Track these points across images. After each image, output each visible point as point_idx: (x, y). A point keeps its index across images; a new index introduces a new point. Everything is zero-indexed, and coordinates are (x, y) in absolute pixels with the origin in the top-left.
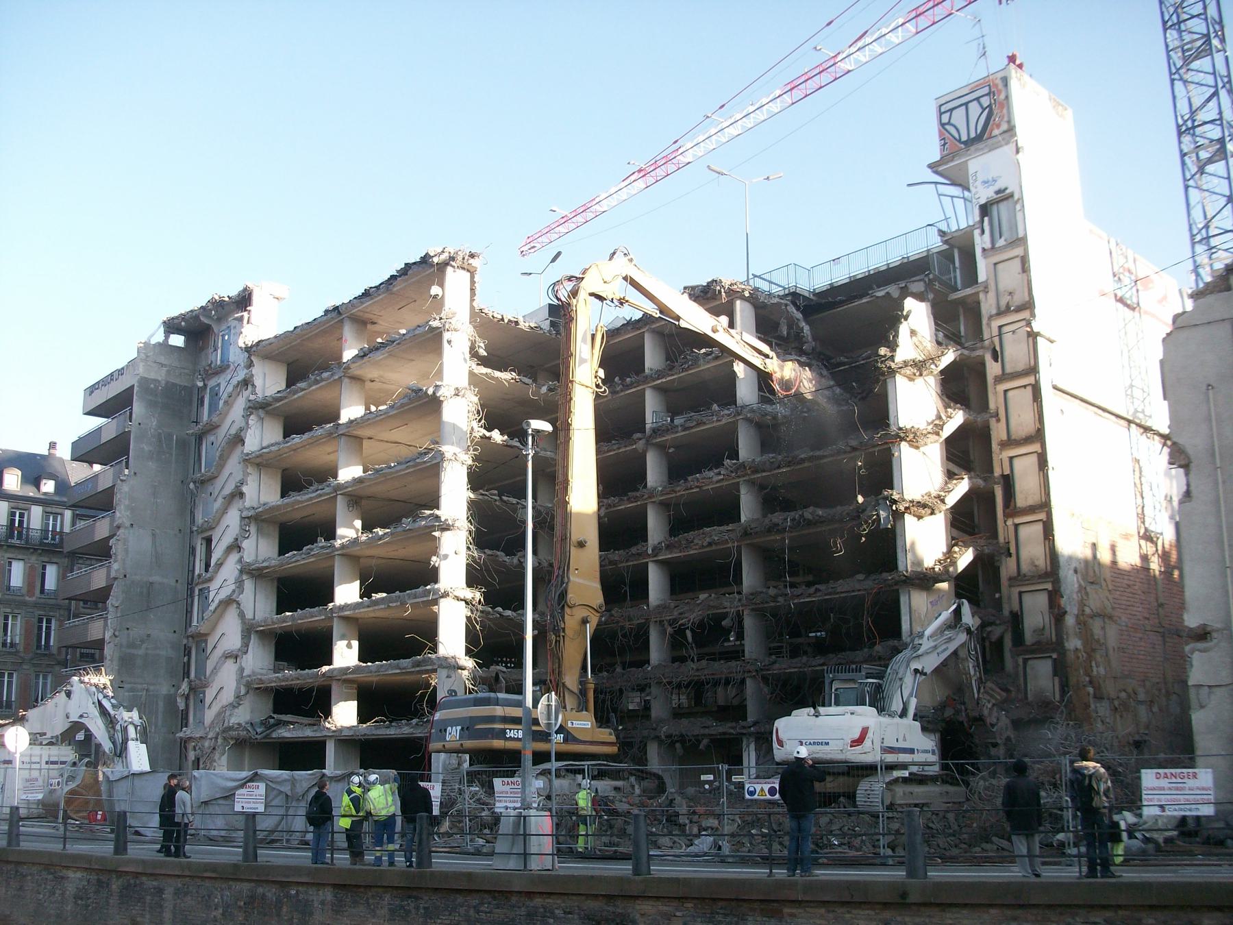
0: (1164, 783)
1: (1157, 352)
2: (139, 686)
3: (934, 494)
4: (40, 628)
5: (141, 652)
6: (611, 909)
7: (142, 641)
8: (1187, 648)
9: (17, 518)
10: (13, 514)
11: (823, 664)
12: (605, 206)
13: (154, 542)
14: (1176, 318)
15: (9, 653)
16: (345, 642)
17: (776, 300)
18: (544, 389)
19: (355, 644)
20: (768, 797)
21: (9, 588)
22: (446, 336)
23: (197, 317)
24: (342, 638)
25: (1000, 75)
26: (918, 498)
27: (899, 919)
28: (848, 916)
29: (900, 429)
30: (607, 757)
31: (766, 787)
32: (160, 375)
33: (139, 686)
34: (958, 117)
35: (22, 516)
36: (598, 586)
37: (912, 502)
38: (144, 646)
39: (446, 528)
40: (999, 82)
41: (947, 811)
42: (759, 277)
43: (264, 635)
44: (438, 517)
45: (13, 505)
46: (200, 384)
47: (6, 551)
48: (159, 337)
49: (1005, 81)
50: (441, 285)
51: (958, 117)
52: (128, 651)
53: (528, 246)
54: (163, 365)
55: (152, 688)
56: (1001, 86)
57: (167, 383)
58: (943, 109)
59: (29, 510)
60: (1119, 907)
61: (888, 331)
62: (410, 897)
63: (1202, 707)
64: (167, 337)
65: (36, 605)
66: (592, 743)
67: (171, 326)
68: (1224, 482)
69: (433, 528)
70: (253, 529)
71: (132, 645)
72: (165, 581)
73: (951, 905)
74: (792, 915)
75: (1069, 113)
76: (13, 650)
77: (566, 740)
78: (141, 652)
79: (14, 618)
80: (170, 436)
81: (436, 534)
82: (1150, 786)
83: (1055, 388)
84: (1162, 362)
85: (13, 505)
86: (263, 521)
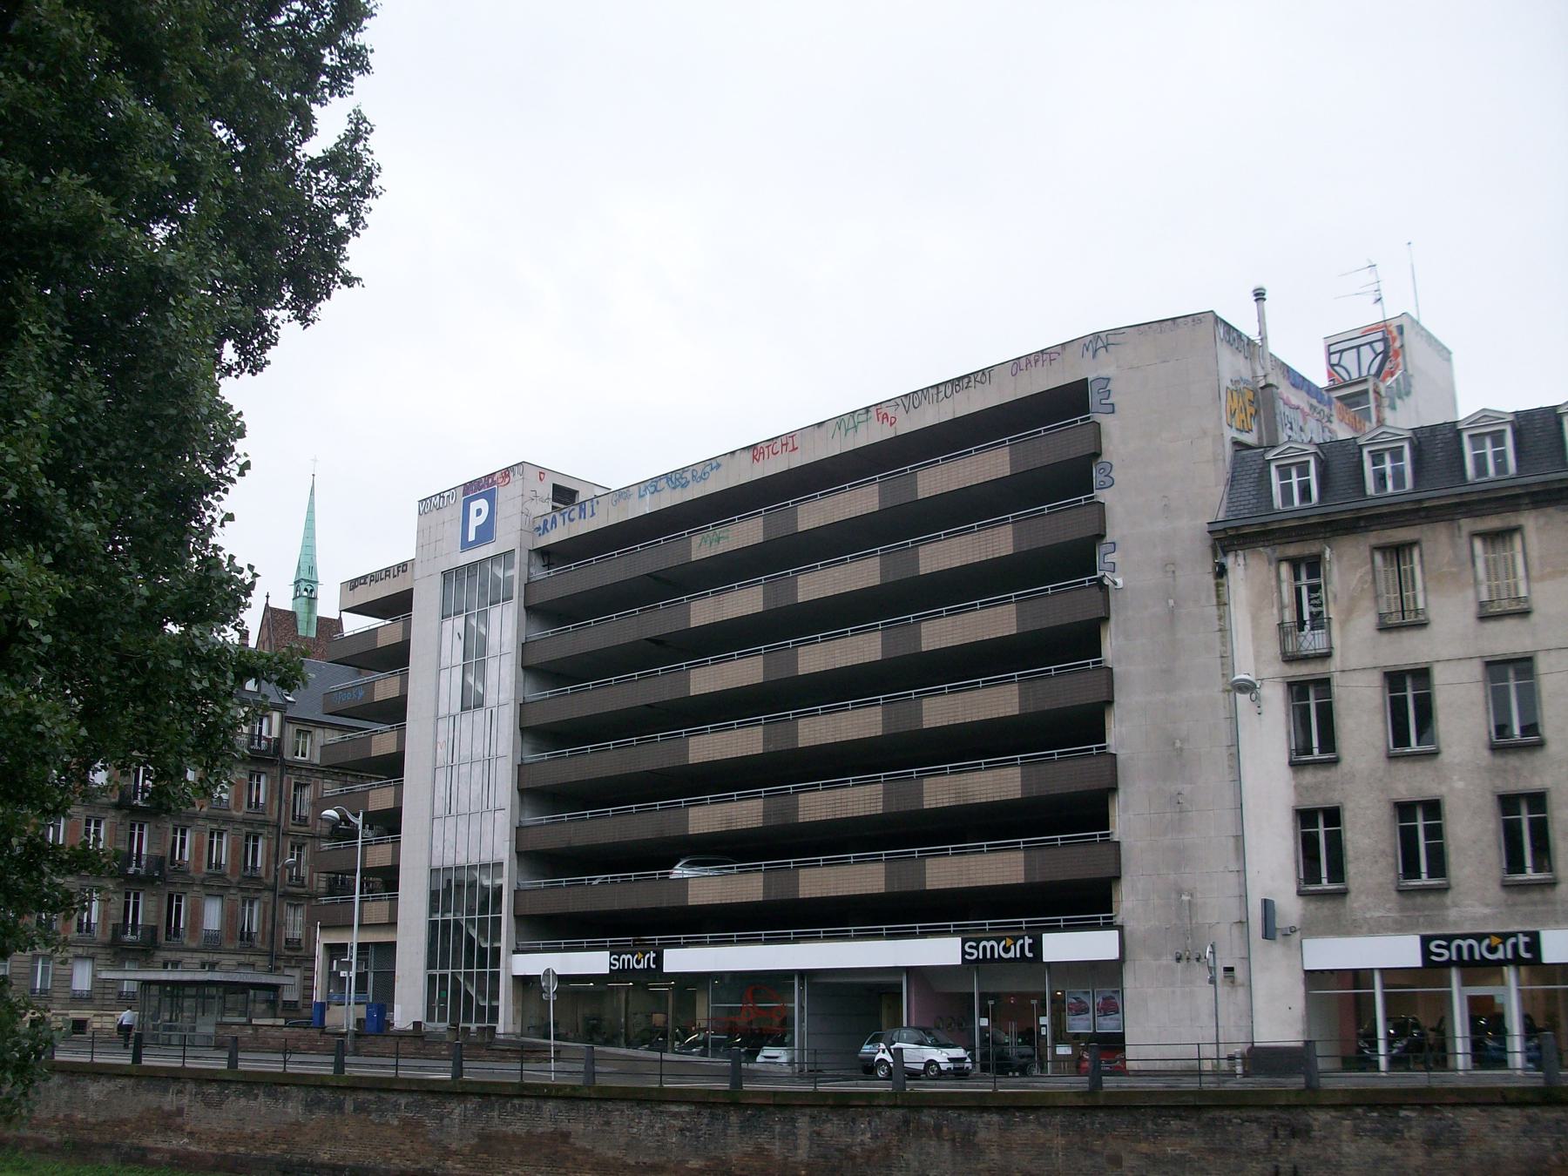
4: (132, 835)
25: (1396, 323)
34: (1349, 359)
41: (298, 1040)
51: (1349, 359)
56: (1395, 333)
58: (1333, 349)
65: (244, 822)
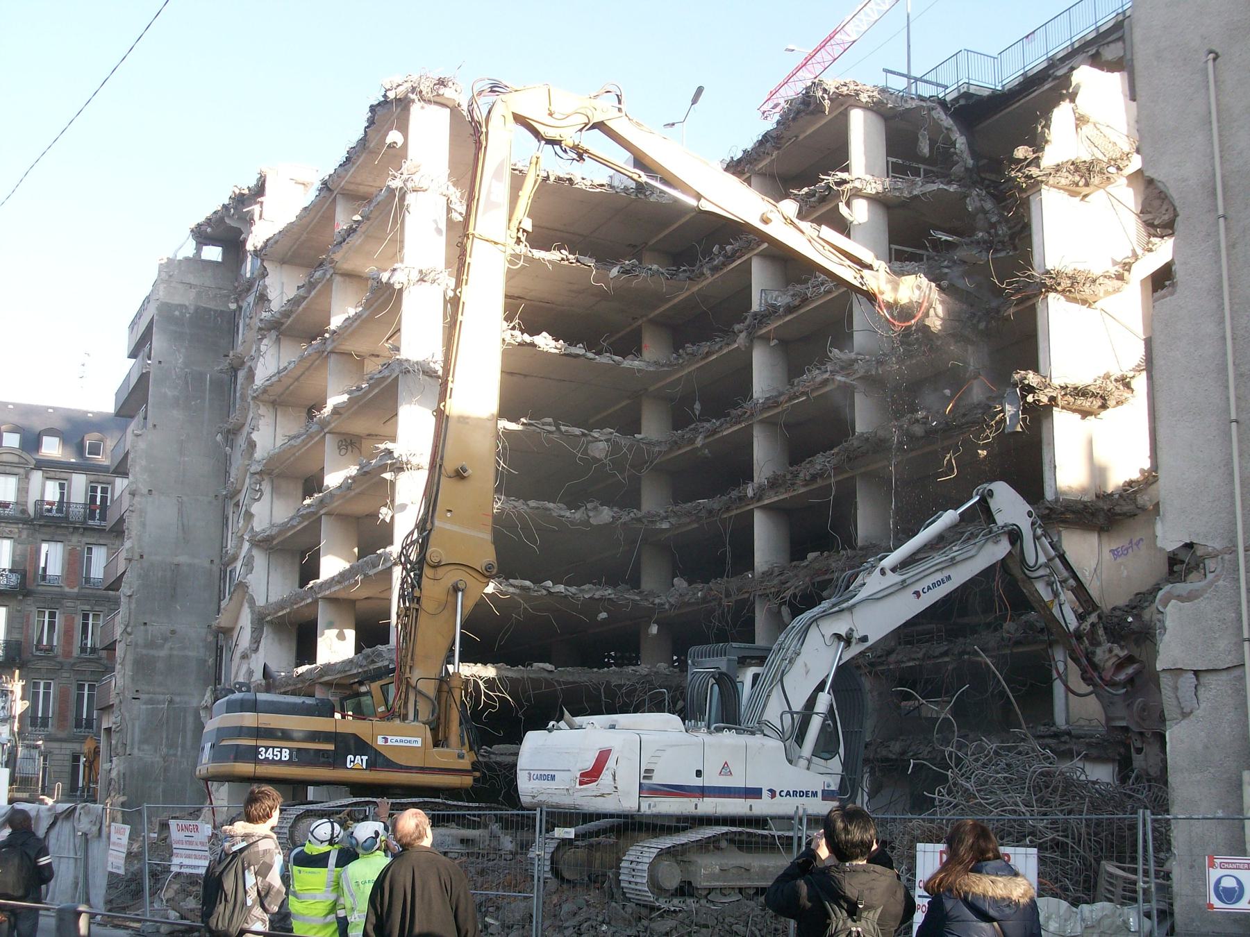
2: (161, 697)
3: (1117, 374)
5: (163, 653)
7: (166, 639)
9: (99, 495)
10: (94, 490)
11: (945, 654)
12: (852, 32)
13: (181, 513)
15: (89, 660)
16: (336, 631)
17: (914, 104)
18: (615, 271)
19: (351, 634)
21: (88, 580)
22: (410, 199)
23: (221, 220)
24: (330, 625)
26: (1081, 380)
29: (1048, 272)
30: (453, 793)
32: (186, 298)
33: (161, 697)
35: (104, 491)
36: (487, 536)
37: (1064, 388)
38: (168, 645)
39: (399, 468)
42: (921, 80)
44: (389, 453)
45: (92, 478)
46: (233, 306)
47: (83, 534)
48: (189, 249)
50: (404, 129)
52: (145, 652)
53: (771, 104)
54: (191, 286)
55: (177, 699)
57: (197, 308)
59: (112, 483)
61: (1036, 120)
63: (1185, 715)
64: (199, 250)
66: (422, 770)
67: (202, 235)
68: (1231, 246)
69: (384, 468)
70: (266, 487)
71: (151, 644)
72: (196, 561)
76: (95, 656)
77: (371, 765)
78: (163, 653)
79: (96, 616)
80: (201, 376)
81: (388, 476)
85: (92, 478)
86: (278, 476)
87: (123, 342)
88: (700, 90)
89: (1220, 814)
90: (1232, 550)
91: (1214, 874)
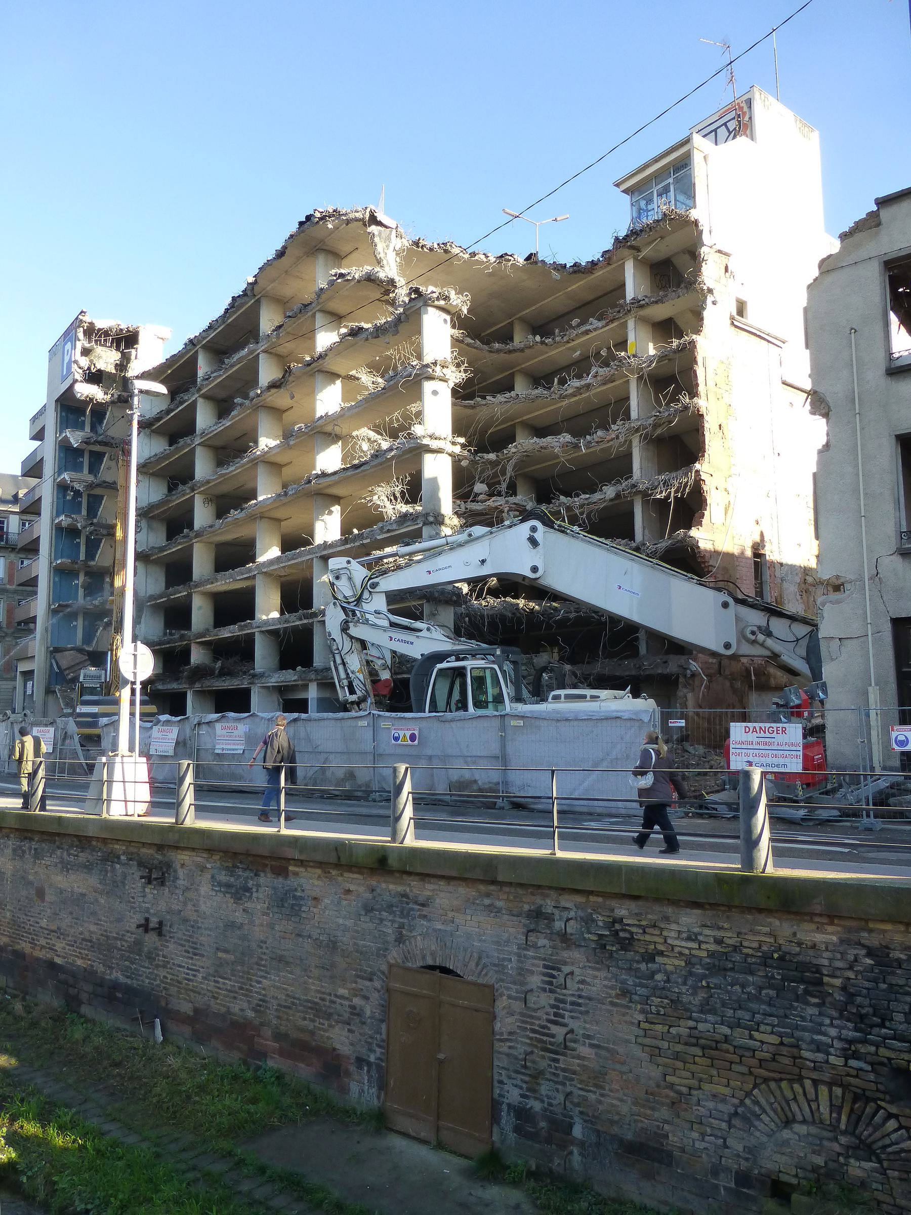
0: (752, 737)
1: (802, 299)
6: (160, 857)
8: (819, 600)
14: (822, 263)
20: (410, 742)
27: (384, 885)
28: (340, 878)
31: (408, 734)
40: (744, 105)
43: (156, 608)
49: (749, 102)
56: (746, 109)
60: (591, 893)
62: (26, 838)
63: (832, 660)
68: (862, 429)
73: (428, 875)
74: (296, 874)
75: (815, 136)
82: (738, 740)
83: (784, 383)
84: (806, 310)
87: (25, 430)
88: (720, 426)
89: (853, 707)
90: (861, 579)
91: (894, 735)
